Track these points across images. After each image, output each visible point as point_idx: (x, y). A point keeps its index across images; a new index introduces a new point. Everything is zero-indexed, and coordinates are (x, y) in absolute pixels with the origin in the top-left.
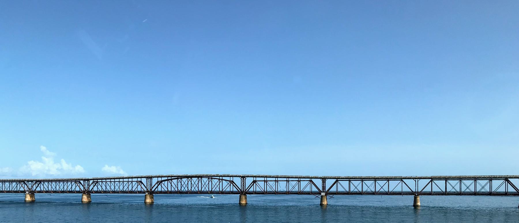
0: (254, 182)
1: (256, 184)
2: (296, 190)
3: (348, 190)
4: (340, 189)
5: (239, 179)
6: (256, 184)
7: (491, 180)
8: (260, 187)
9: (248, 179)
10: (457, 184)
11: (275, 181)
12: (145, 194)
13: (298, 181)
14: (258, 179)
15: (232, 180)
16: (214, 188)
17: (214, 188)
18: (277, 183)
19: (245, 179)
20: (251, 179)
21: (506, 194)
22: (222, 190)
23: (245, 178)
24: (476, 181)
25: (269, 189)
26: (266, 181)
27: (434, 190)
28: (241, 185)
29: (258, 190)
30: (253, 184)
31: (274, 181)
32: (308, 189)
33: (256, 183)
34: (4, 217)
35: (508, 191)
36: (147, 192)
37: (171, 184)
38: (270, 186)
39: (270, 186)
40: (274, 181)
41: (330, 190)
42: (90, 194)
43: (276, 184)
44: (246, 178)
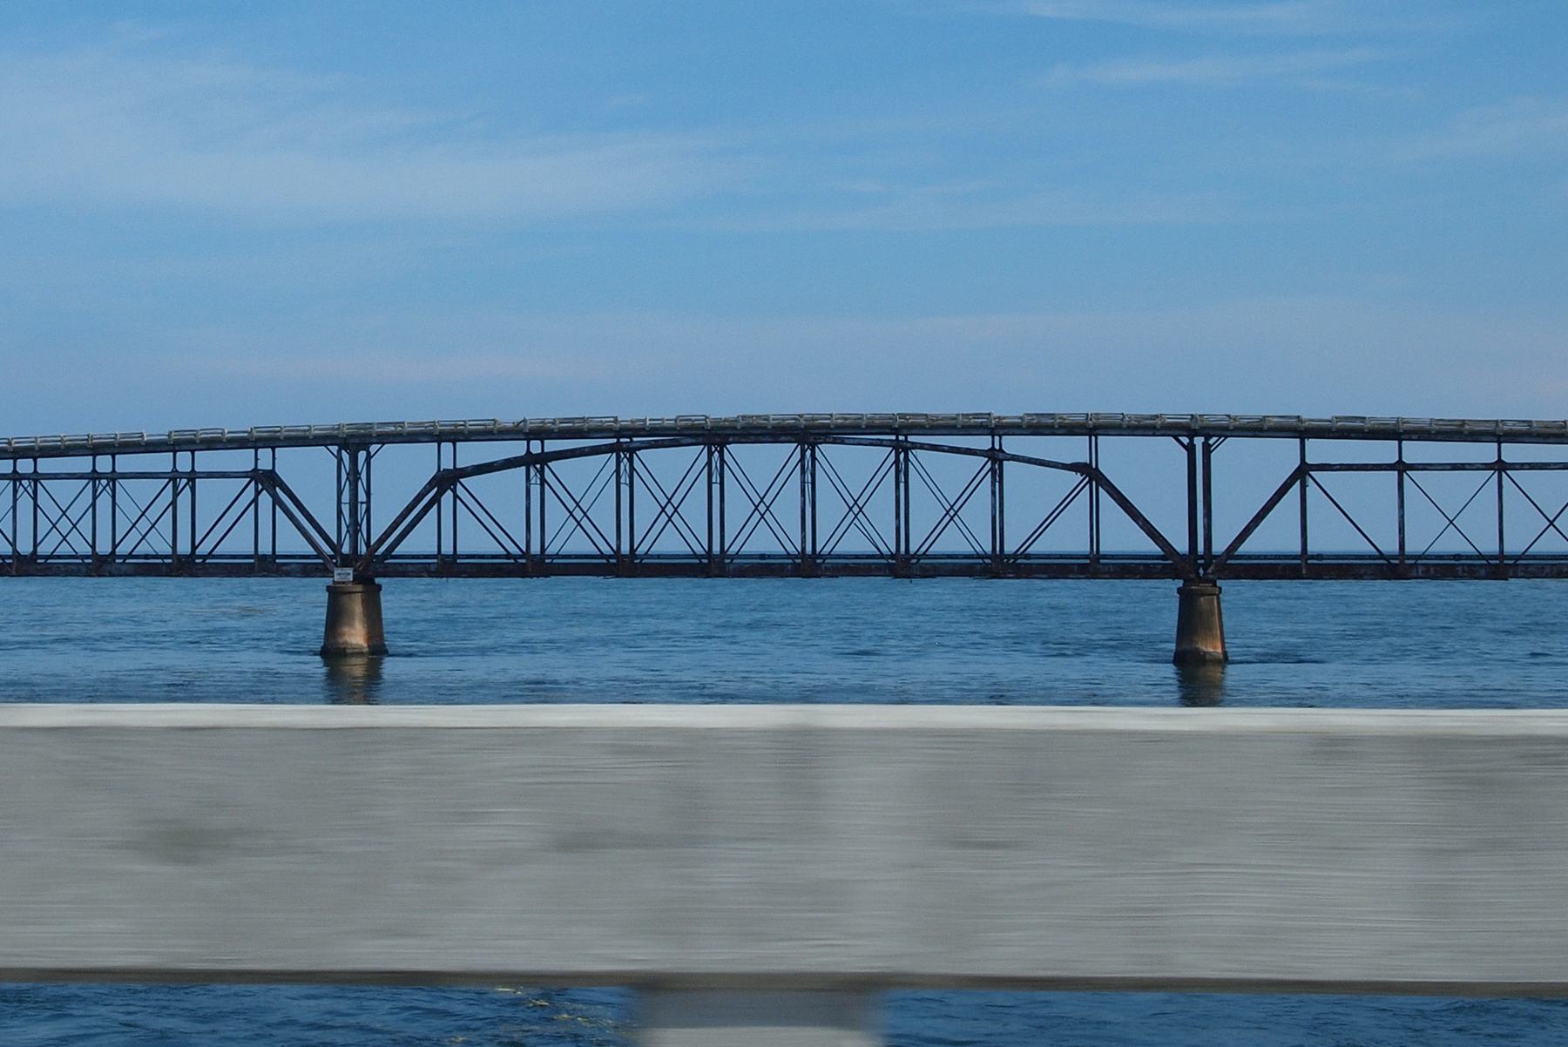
0: (446, 480)
1: (456, 497)
2: (979, 549)
3: (1390, 545)
4: (1330, 538)
5: (1170, 451)
6: (456, 497)
7: (722, 446)
8: (488, 521)
9: (1228, 453)
10: (87, 485)
11: (94, 476)
12: (329, 581)
13: (527, 460)
14: (471, 453)
15: (265, 465)
16: (134, 537)
17: (134, 537)
18: (104, 501)
19: (369, 457)
20: (421, 462)
21: (1093, 566)
22: (189, 550)
23: (362, 455)
24: (906, 459)
25: (569, 541)
26: (182, 475)
27: (1318, 544)
28: (368, 502)
29: (474, 541)
30: (436, 500)
31: (1487, 467)
32: (1068, 538)
33: (454, 491)
34: (1456, 675)
35: (1101, 549)
36: (346, 561)
37: (35, 498)
38: (585, 523)
39: (585, 523)
40: (1487, 467)
41: (1243, 549)
42: (378, 580)
43: (174, 503)
44: (373, 448)
